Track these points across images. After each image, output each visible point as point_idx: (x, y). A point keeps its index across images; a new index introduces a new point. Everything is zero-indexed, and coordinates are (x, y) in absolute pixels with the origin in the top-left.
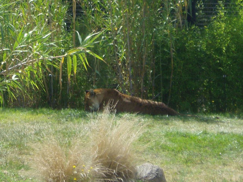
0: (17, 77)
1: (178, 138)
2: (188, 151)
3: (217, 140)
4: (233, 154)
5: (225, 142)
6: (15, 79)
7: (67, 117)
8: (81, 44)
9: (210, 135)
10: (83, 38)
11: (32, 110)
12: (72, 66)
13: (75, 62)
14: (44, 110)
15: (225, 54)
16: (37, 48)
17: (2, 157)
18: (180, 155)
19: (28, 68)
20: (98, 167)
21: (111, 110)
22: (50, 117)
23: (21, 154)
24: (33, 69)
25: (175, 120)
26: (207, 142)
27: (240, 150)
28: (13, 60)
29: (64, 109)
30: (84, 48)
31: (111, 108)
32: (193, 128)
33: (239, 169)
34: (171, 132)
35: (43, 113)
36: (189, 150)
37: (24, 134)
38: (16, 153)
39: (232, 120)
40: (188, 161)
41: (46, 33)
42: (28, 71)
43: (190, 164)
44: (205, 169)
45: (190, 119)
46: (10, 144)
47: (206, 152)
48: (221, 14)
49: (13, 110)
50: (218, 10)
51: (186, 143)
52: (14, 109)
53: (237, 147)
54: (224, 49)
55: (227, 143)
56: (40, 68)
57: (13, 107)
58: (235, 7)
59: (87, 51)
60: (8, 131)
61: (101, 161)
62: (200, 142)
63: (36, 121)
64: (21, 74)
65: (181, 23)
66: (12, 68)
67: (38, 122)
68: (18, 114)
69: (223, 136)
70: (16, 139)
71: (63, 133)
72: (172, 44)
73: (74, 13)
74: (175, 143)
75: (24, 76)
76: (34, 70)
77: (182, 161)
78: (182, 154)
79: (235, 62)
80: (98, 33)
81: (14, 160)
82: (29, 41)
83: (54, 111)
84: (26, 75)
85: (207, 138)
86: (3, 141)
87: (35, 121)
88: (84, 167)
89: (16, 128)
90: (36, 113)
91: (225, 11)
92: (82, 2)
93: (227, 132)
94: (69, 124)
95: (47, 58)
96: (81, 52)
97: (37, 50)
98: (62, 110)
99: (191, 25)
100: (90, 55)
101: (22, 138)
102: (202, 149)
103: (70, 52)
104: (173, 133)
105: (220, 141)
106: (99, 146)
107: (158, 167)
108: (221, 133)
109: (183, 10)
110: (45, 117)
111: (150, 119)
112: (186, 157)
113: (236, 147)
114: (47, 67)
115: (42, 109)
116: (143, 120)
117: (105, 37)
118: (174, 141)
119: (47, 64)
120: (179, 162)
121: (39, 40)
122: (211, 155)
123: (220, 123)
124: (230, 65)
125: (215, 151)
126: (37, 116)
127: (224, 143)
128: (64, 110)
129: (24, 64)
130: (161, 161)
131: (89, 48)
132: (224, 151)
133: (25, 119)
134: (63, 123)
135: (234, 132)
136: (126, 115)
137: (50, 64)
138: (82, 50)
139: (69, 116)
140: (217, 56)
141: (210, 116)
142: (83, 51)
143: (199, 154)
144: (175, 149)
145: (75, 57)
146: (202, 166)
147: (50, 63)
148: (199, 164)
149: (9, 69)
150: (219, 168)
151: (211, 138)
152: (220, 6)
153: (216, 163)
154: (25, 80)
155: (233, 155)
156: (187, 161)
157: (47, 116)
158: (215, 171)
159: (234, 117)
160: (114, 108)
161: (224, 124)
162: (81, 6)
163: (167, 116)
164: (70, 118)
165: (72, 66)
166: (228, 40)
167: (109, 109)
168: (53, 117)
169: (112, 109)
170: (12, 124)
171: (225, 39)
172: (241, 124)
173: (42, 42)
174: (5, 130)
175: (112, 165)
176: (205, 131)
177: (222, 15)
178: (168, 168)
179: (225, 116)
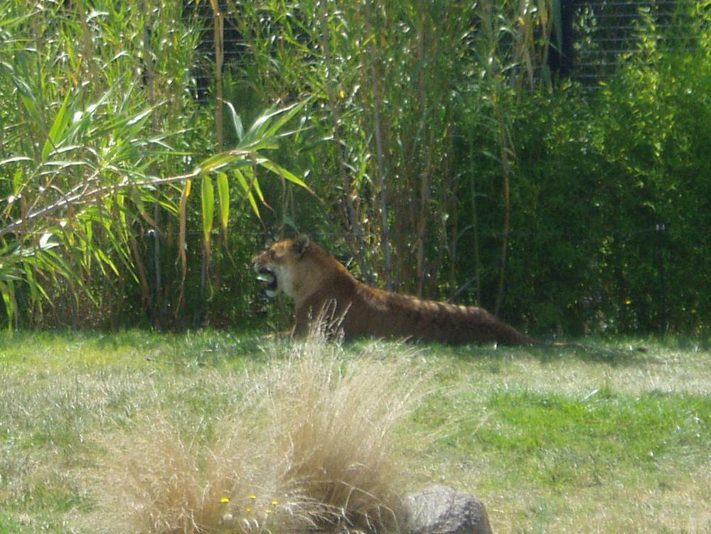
0: (54, 238)
2: (557, 450)
4: (688, 454)
5: (665, 421)
6: (49, 244)
7: (202, 354)
8: (241, 140)
9: (619, 401)
10: (247, 124)
12: (217, 205)
13: (223, 194)
14: (136, 334)
16: (111, 155)
19: (88, 213)
20: (294, 501)
21: (330, 331)
23: (68, 465)
25: (518, 357)
28: (42, 189)
29: (194, 329)
30: (250, 152)
31: (329, 328)
32: (571, 380)
33: (706, 499)
34: (507, 394)
36: (559, 445)
41: (138, 111)
42: (87, 221)
43: (563, 487)
46: (37, 437)
47: (610, 451)
48: (646, 45)
50: (637, 32)
51: (550, 426)
53: (700, 434)
54: (659, 148)
57: (44, 329)
59: (257, 160)
60: (30, 398)
64: (66, 229)
65: (531, 73)
67: (117, 372)
69: (659, 402)
70: (55, 423)
72: (507, 138)
73: (218, 48)
76: (103, 219)
78: (541, 458)
81: (48, 482)
82: (89, 132)
86: (15, 429)
88: (253, 499)
90: (111, 345)
92: (241, 19)
95: (142, 182)
96: (241, 163)
97: (112, 159)
99: (561, 78)
100: (267, 172)
102: (598, 441)
104: (512, 395)
106: (295, 437)
108: (651, 394)
109: (537, 35)
110: (137, 354)
112: (551, 466)
113: (699, 435)
114: (141, 208)
115: (129, 332)
117: (310, 118)
118: (514, 420)
119: (143, 199)
121: (118, 129)
123: (648, 365)
126: (115, 354)
127: (663, 423)
131: (263, 153)
134: (192, 373)
136: (374, 346)
137: (150, 200)
138: (243, 157)
140: (637, 170)
141: (621, 346)
142: (248, 160)
143: (590, 457)
144: (518, 444)
145: (223, 179)
147: (151, 197)
149: (31, 216)
152: (643, 23)
155: (689, 457)
156: (553, 478)
157: (144, 351)
159: (691, 347)
162: (237, 29)
163: (495, 346)
165: (217, 205)
166: (668, 122)
169: (332, 330)
173: (126, 135)
177: (650, 49)
178: (500, 499)
179: (664, 344)
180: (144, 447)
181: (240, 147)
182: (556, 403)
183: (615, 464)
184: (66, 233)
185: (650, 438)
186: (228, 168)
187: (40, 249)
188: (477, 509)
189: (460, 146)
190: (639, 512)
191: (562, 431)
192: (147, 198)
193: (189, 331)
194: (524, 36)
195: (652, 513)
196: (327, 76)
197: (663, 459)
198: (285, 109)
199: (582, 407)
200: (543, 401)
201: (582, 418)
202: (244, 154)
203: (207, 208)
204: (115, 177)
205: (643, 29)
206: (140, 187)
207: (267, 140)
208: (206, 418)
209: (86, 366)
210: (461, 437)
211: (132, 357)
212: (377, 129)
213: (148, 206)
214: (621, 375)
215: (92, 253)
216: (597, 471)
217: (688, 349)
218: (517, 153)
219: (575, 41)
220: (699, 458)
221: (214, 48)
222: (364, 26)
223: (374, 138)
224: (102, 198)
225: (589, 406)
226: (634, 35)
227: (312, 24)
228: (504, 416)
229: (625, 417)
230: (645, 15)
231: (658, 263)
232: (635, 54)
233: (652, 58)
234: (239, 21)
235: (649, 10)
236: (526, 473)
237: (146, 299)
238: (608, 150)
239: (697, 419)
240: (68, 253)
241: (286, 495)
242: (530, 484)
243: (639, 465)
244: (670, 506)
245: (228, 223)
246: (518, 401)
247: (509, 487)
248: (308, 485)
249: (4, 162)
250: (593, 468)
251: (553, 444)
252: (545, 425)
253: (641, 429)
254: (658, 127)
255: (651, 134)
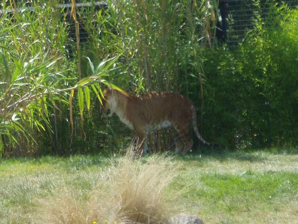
1: (217, 182)
2: (230, 197)
3: (264, 181)
4: (286, 197)
5: (275, 183)
6: (16, 119)
7: (77, 165)
8: (94, 72)
9: (255, 176)
11: (34, 160)
13: (87, 95)
14: (49, 158)
15: (266, 76)
16: (40, 80)
17: (3, 217)
18: (221, 202)
19: (31, 105)
20: (124, 222)
21: (136, 150)
22: (57, 166)
23: (25, 212)
24: (37, 106)
25: (210, 160)
26: (253, 184)
27: (294, 192)
28: (12, 95)
29: (73, 155)
30: (98, 77)
31: (136, 149)
32: (234, 168)
33: (295, 215)
34: (208, 175)
35: (47, 161)
36: (231, 195)
37: (27, 188)
38: (19, 212)
39: (280, 155)
40: (231, 209)
41: (51, 61)
42: (31, 108)
43: (234, 212)
44: (253, 217)
45: (228, 159)
46: (11, 202)
47: (252, 197)
48: (258, 27)
49: (10, 161)
50: (254, 22)
51: (227, 187)
52: (11, 160)
53: (290, 188)
54: (265, 70)
55: (277, 183)
56: (45, 105)
57: (9, 158)
58: (274, 18)
59: (101, 80)
60: (7, 186)
61: (127, 214)
62: (244, 185)
63: (41, 171)
64: (23, 112)
65: (210, 41)
66: (11, 106)
67: (42, 174)
68: (17, 165)
69: (272, 176)
70: (19, 195)
71: (75, 184)
72: (201, 68)
73: (77, 37)
74: (214, 187)
75: (26, 116)
76: (38, 107)
77: (225, 209)
78: (224, 201)
79: (279, 85)
80: (114, 59)
81: (17, 220)
83: (61, 159)
84: (28, 114)
85: (252, 180)
86: (2, 199)
87: (39, 172)
88: (106, 222)
89: (17, 182)
91: (263, 23)
92: (86, 24)
93: (276, 171)
94: (81, 173)
95: (53, 91)
96: (94, 82)
97: (41, 82)
98: (71, 157)
99: (222, 43)
100: (105, 85)
101: (25, 194)
102: (247, 193)
103: (80, 83)
104: (210, 175)
105: (268, 181)
106: (123, 195)
107: (197, 217)
108: (268, 172)
109: (211, 25)
110: (50, 166)
111: (180, 161)
112: (229, 204)
113: (290, 188)
114: (53, 102)
115: (46, 157)
116: (171, 163)
118: (212, 185)
119: (54, 98)
120: (221, 210)
122: (259, 200)
123: (265, 161)
124: (273, 89)
125: (263, 194)
126: (41, 167)
127: (274, 184)
128: (73, 157)
129: (25, 100)
130: (198, 211)
131: (103, 77)
132: (274, 194)
133: (26, 171)
134: (74, 173)
135: (284, 170)
136: (151, 159)
137: (58, 99)
138: (95, 80)
139: (80, 164)
140: (257, 80)
141: (253, 154)
142: (97, 81)
143: (244, 200)
144: (214, 195)
145: (87, 90)
146: (249, 213)
148: (245, 211)
149: (8, 107)
150: (270, 215)
151: (257, 179)
152: (256, 18)
153: (266, 209)
154: (28, 120)
155: (286, 197)
156: (230, 209)
157: (53, 165)
158: (266, 218)
159: (283, 153)
160: (139, 147)
161: (272, 162)
162: (85, 28)
163: (200, 156)
164: (80, 166)
165: (85, 99)
166: (268, 59)
167: (133, 150)
168: (60, 166)
169: (137, 150)
170: (11, 177)
171: (264, 58)
172: (292, 161)
174: (3, 185)
175: (140, 218)
176: (250, 171)
177: (259, 28)
178: (208, 219)
179: (271, 152)
180: (59, 202)
181: (93, 75)
182: (229, 178)
183: (255, 202)
184: (22, 114)
185: (269, 190)
186: (89, 84)
187: (12, 121)
188: (200, 222)
189: (181, 73)
190: (267, 221)
191: (232, 189)
192: (56, 98)
193: (71, 155)
194: (206, 25)
195: (273, 222)
196: (124, 46)
197: (275, 199)
198: (111, 59)
199: (240, 179)
200: (223, 177)
201: (240, 184)
202: (95, 78)
203: (81, 102)
204: (41, 90)
205: (256, 20)
206: (53, 94)
207: (105, 72)
208: (82, 191)
209: (29, 172)
210: (190, 193)
211: (48, 167)
212: (146, 68)
213: (56, 101)
214: (255, 165)
215: (34, 122)
216: (248, 205)
217: (281, 153)
218: (206, 75)
219: (227, 29)
220: (290, 198)
221: (76, 37)
222: (139, 24)
223: (145, 71)
224: (37, 99)
225: (243, 178)
226: (253, 23)
227: (116, 24)
228: (207, 184)
229: (258, 182)
230: (257, 14)
231: (267, 118)
232: (253, 31)
233: (260, 32)
234: (85, 25)
235: (258, 12)
236: (218, 207)
237: (52, 143)
238: (243, 72)
239: (289, 182)
240: (23, 122)
241: (120, 220)
242: (220, 212)
243: (265, 202)
244: (280, 218)
245: (90, 107)
246: (212, 177)
247: (211, 213)
248: (129, 215)
249: (2, 83)
250: (246, 204)
251: (228, 195)
252: (225, 187)
253: (265, 187)
254: (264, 61)
255: (261, 64)
